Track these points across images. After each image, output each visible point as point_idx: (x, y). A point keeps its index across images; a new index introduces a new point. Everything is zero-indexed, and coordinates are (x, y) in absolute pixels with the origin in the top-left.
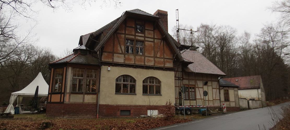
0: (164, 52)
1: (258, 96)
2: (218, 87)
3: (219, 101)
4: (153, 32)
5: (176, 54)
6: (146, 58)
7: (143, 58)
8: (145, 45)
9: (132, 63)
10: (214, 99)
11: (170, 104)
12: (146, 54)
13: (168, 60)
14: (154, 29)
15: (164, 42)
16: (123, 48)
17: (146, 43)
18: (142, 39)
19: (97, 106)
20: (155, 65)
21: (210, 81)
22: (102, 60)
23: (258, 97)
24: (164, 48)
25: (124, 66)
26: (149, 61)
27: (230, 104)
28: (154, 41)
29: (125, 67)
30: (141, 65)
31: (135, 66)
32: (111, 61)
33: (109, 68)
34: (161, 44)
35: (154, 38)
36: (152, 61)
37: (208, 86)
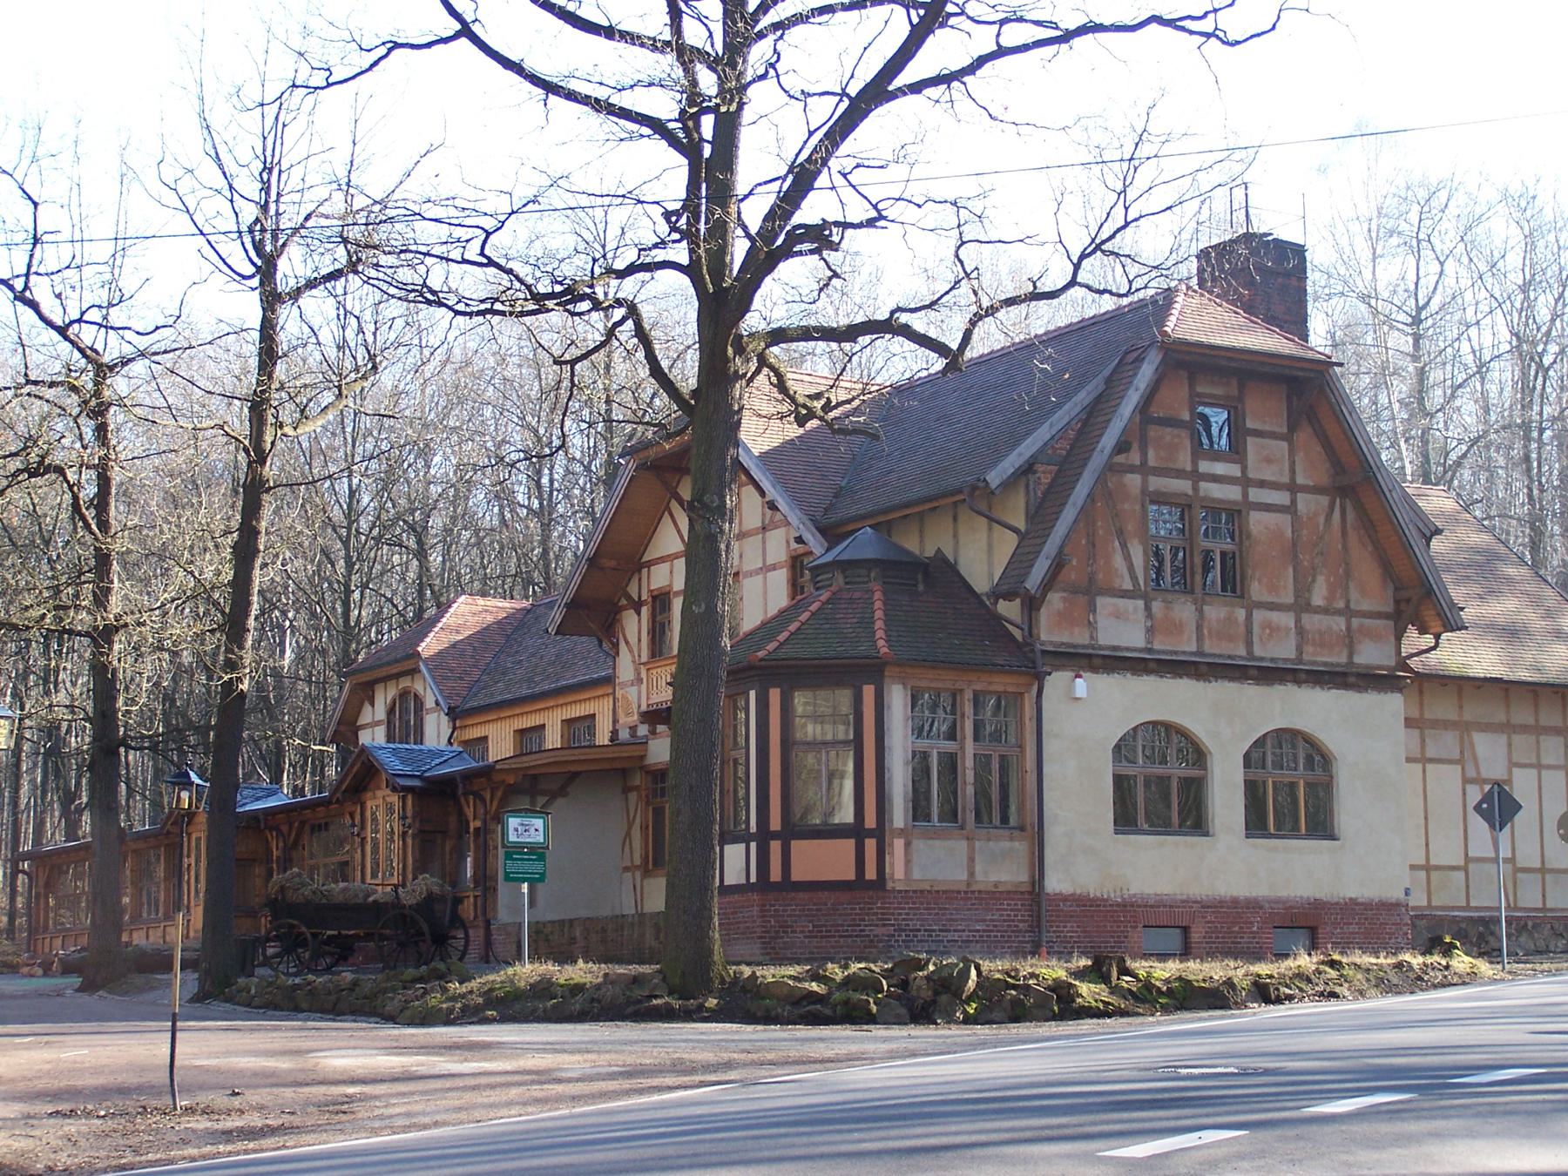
6: (1259, 616)
9: (1186, 645)
12: (1257, 591)
13: (1367, 622)
14: (1292, 428)
22: (1043, 637)
24: (1345, 548)
28: (1294, 502)
29: (1152, 678)
34: (1328, 518)
35: (1293, 488)
36: (1288, 629)
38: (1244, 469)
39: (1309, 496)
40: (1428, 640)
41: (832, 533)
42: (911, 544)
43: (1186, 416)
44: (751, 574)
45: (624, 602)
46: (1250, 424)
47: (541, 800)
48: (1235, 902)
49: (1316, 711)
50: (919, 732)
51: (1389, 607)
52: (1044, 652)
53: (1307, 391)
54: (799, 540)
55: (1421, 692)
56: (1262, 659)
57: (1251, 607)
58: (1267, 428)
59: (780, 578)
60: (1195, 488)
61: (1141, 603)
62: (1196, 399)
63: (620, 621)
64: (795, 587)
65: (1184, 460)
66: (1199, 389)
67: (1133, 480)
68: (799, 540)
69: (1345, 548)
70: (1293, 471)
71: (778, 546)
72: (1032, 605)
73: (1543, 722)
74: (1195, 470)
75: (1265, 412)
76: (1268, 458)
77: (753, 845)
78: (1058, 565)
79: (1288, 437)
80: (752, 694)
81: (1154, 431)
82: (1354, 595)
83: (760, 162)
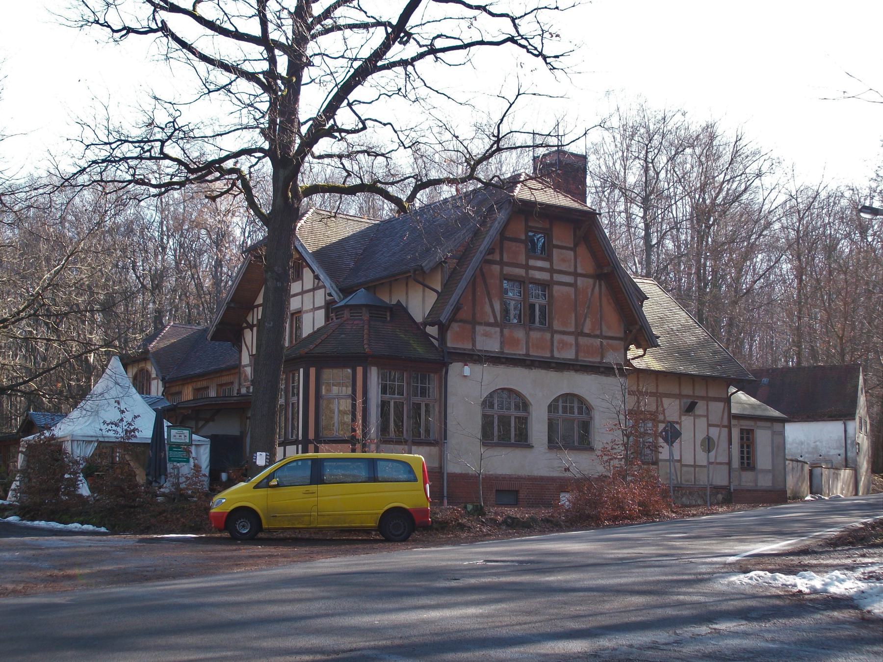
0: (601, 318)
1: (842, 451)
2: (725, 422)
3: (726, 467)
4: (572, 253)
5: (637, 327)
6: (557, 337)
7: (548, 336)
8: (551, 296)
9: (520, 351)
10: (712, 460)
11: (130, 432)
12: (557, 326)
13: (610, 341)
14: (576, 245)
15: (603, 283)
16: (497, 307)
17: (556, 288)
18: (545, 276)
19: (443, 478)
20: (580, 358)
21: (702, 398)
22: (449, 345)
23: (843, 456)
24: (601, 306)
25: (503, 363)
26: (564, 345)
27: (756, 481)
28: (576, 281)
29: (502, 366)
30: (543, 357)
31: (528, 362)
32: (470, 347)
33: (467, 370)
34: (593, 290)
35: (575, 274)
36: (571, 345)
37: (695, 416)
38: (552, 264)
39: (583, 279)
40: (640, 352)
41: (346, 291)
42: (386, 299)
43: (523, 237)
44: (307, 312)
45: (245, 325)
46: (555, 242)
47: (201, 423)
48: (542, 478)
49: (586, 385)
50: (384, 391)
51: (621, 334)
52: (449, 352)
53: (584, 225)
54: (330, 295)
55: (638, 378)
56: (558, 359)
57: (554, 332)
58: (564, 244)
59: (322, 313)
60: (527, 273)
61: (498, 329)
62: (528, 229)
63: (243, 334)
64: (327, 317)
65: (522, 259)
66: (530, 224)
67: (496, 268)
68: (330, 295)
69: (601, 306)
70: (576, 267)
71: (320, 298)
72: (443, 329)
73: (710, 395)
74: (527, 264)
75: (562, 236)
76: (563, 259)
77: (300, 446)
78: (457, 308)
79: (573, 249)
80: (301, 370)
81: (507, 244)
82: (604, 328)
83: (310, 102)
